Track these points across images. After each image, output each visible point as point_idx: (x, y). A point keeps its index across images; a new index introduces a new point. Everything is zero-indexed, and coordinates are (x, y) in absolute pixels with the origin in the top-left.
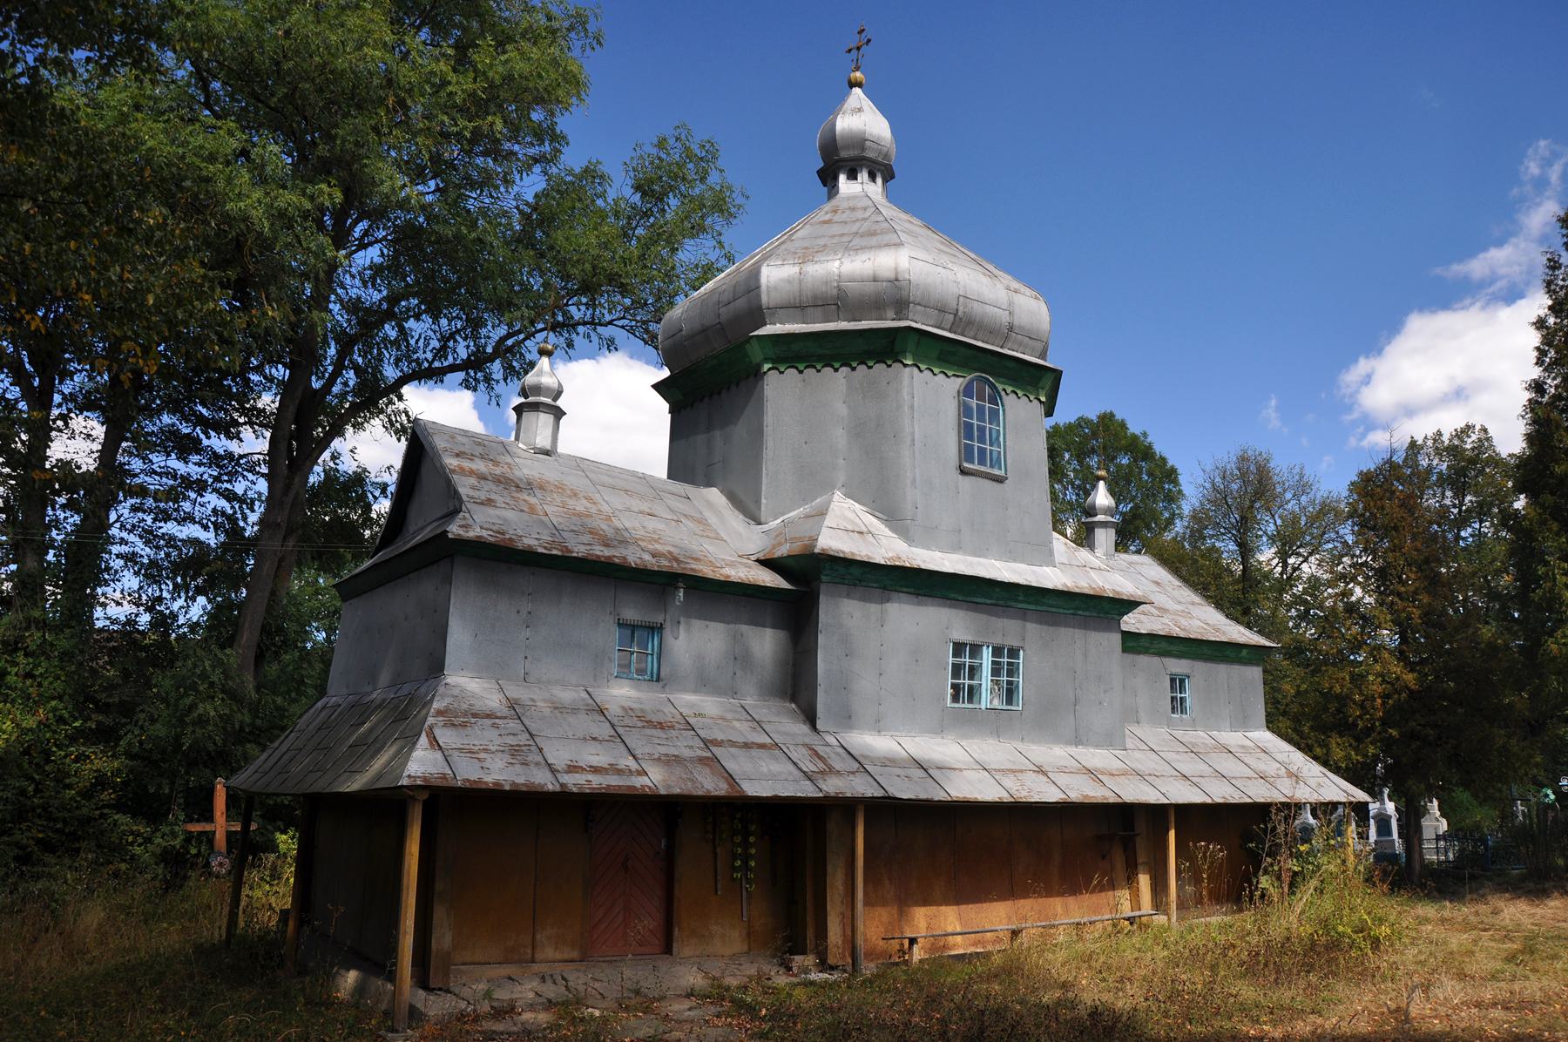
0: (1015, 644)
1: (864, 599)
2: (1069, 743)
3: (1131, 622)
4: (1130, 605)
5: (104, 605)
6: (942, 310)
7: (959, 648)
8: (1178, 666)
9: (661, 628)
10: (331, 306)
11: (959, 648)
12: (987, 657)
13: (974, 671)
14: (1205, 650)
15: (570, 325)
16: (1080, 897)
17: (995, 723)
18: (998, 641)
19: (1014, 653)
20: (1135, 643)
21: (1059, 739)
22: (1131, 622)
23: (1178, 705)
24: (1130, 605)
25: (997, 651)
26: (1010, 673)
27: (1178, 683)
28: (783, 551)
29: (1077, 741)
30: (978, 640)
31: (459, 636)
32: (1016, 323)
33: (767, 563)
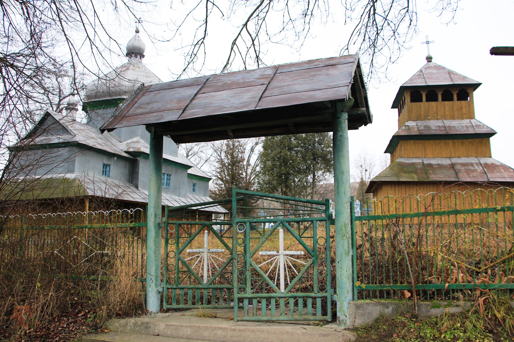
3: (190, 171)
4: (190, 167)
8: (195, 181)
9: (109, 165)
10: (229, 134)
12: (166, 175)
16: (341, 122)
18: (167, 173)
19: (170, 175)
20: (191, 176)
21: (176, 195)
22: (190, 171)
23: (194, 190)
24: (190, 167)
25: (167, 175)
27: (194, 185)
28: (131, 150)
29: (179, 196)
31: (77, 165)
33: (125, 152)
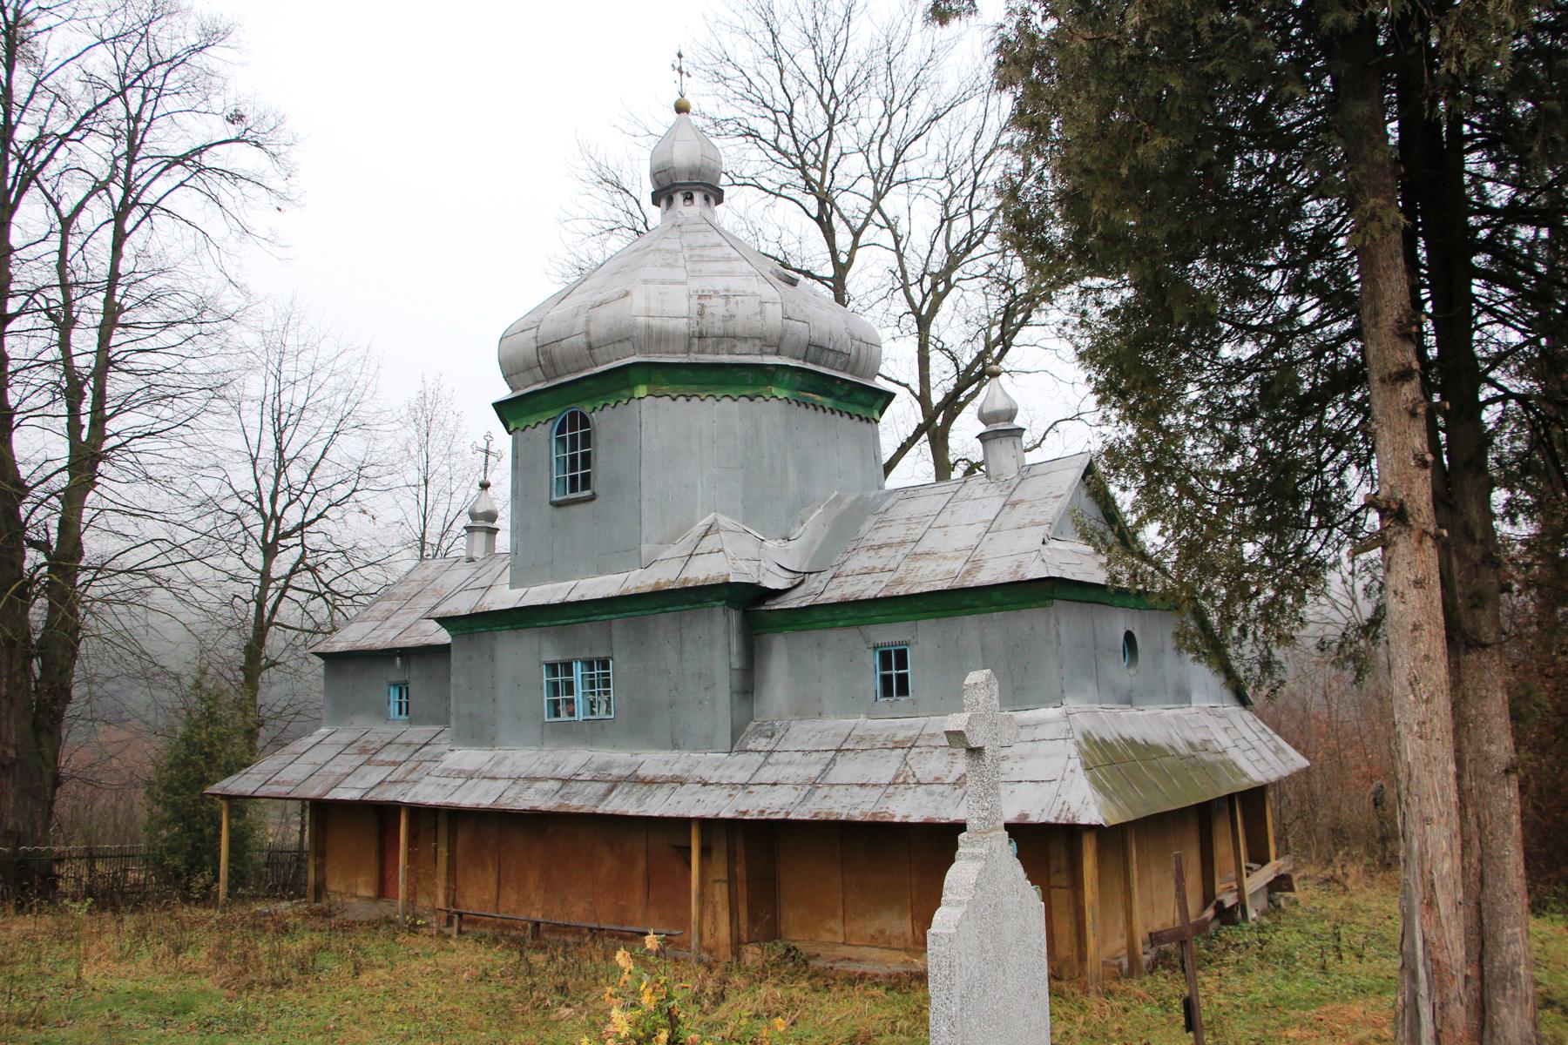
0: (602, 654)
1: (815, 635)
2: (662, 747)
5: (435, 910)
6: (529, 369)
7: (553, 668)
8: (889, 634)
11: (553, 668)
12: (578, 669)
13: (570, 687)
14: (996, 596)
15: (1038, 127)
17: (592, 732)
18: (586, 655)
19: (605, 664)
21: (653, 743)
25: (589, 664)
26: (556, 684)
30: (567, 658)
32: (593, 339)
